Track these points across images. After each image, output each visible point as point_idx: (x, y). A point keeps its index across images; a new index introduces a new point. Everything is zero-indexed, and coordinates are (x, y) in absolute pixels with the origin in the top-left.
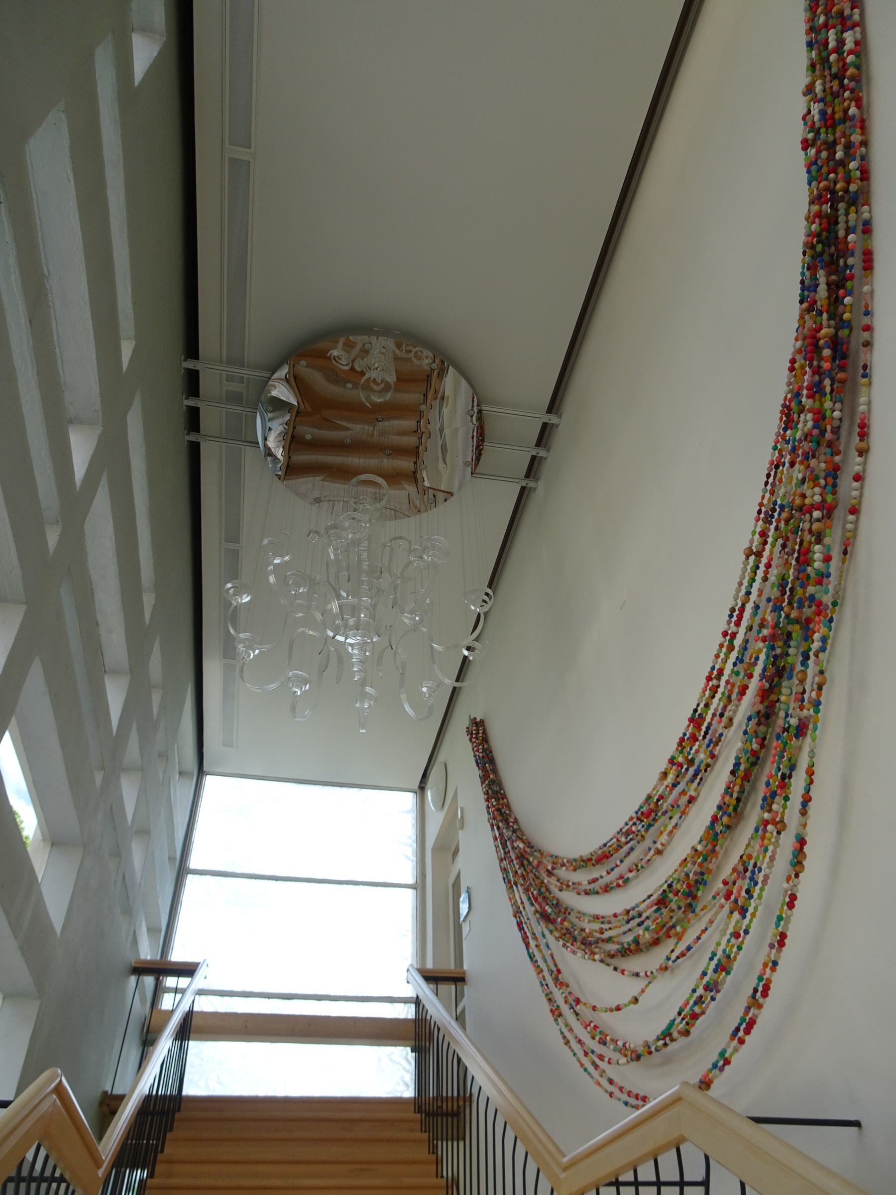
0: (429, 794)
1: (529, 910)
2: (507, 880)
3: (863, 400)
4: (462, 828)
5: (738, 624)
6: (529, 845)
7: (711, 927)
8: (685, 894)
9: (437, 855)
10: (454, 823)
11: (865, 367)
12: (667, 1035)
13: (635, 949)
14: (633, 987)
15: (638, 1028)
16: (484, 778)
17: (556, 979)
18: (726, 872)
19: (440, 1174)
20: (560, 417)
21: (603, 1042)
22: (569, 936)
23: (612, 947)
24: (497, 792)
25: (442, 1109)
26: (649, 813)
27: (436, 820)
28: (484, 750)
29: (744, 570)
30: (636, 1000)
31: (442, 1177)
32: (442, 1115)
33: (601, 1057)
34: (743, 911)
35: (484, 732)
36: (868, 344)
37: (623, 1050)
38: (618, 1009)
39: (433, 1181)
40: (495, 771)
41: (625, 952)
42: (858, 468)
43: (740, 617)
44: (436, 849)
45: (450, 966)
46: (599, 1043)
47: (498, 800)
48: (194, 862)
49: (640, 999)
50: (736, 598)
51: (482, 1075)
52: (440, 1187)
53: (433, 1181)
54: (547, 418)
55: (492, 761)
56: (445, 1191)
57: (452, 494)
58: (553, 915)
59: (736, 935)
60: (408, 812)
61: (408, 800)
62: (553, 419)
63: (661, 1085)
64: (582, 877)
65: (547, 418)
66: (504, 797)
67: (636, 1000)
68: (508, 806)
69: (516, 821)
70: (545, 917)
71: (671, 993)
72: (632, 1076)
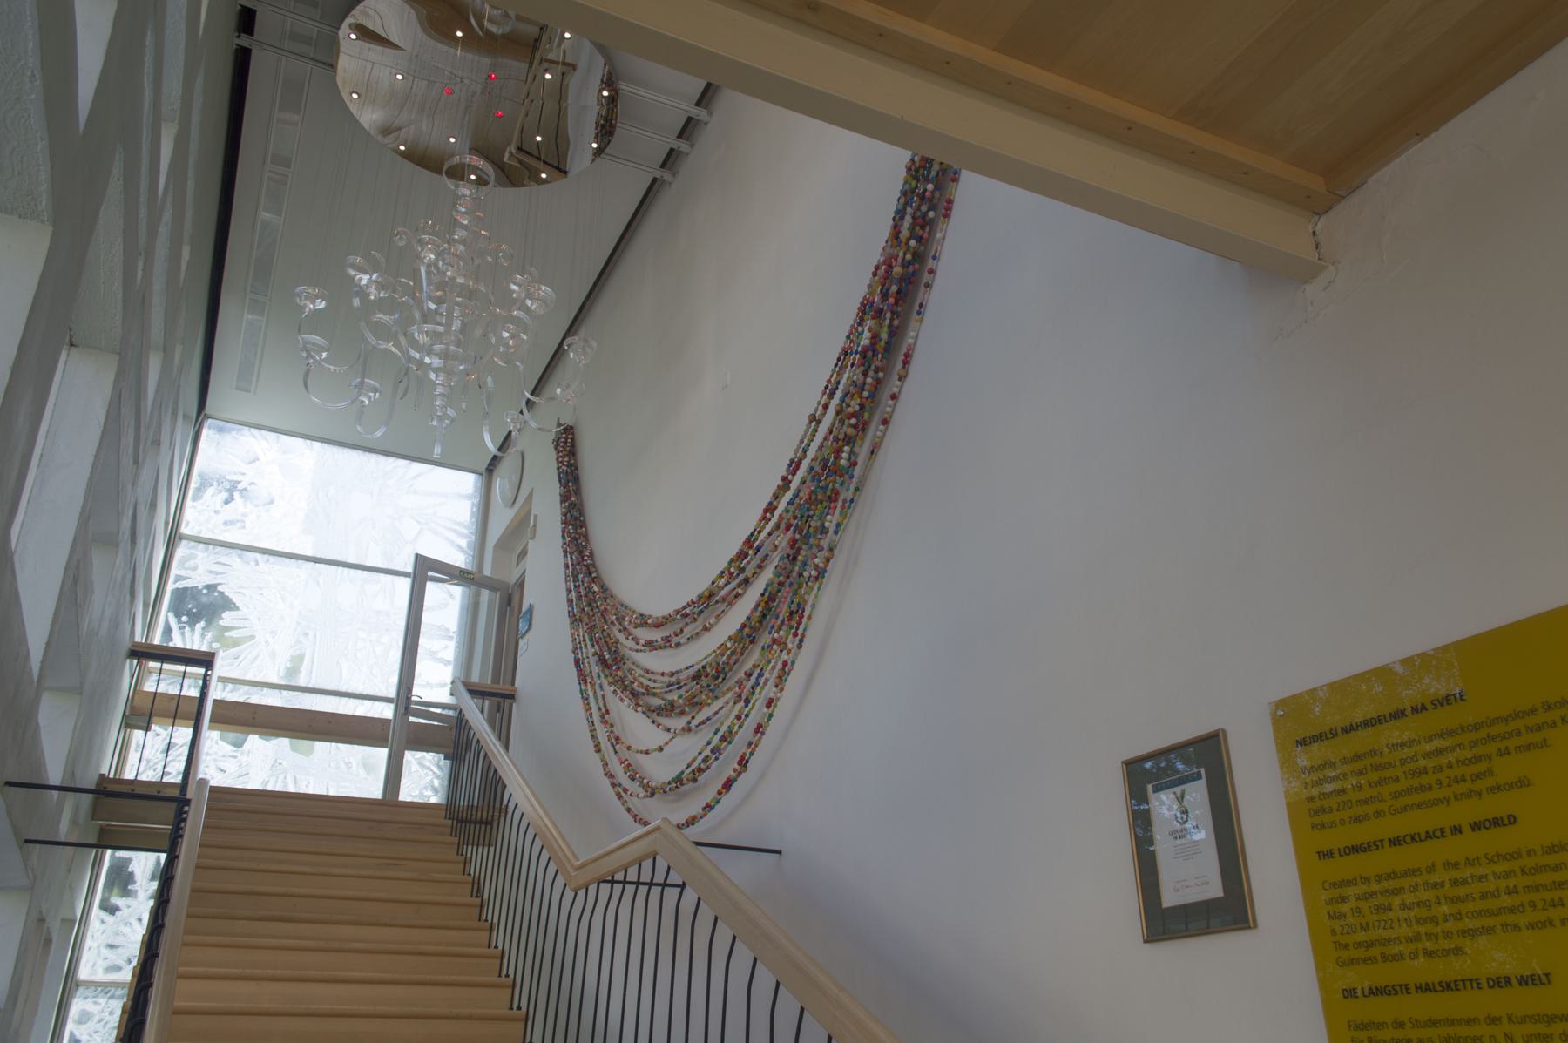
0: (498, 484)
1: (589, 651)
2: (572, 615)
3: (913, 334)
4: (533, 538)
5: (794, 473)
6: (604, 589)
7: (722, 709)
8: (710, 677)
9: (502, 539)
10: (521, 528)
11: (921, 305)
12: (678, 780)
13: (669, 709)
14: (660, 737)
15: (660, 770)
16: (565, 498)
17: (602, 717)
18: (748, 667)
19: (515, 1005)
20: (692, 146)
21: (632, 778)
22: (623, 685)
23: (657, 702)
24: (576, 519)
25: (476, 813)
26: (708, 598)
27: (502, 519)
28: (569, 465)
29: (806, 432)
30: (661, 749)
31: (519, 1008)
32: (481, 822)
33: (625, 790)
34: (747, 701)
35: (573, 445)
36: (928, 285)
37: (645, 787)
38: (647, 752)
39: (469, 900)
40: (578, 492)
41: (659, 711)
42: (895, 390)
43: (797, 467)
44: (502, 545)
45: (502, 687)
46: (630, 780)
47: (575, 528)
48: (184, 530)
49: (664, 749)
50: (796, 451)
51: (520, 792)
52: (516, 1020)
53: (494, 979)
54: (676, 143)
55: (576, 480)
56: (522, 1025)
57: (574, 67)
58: (612, 661)
59: (738, 717)
60: (468, 497)
61: (467, 482)
62: (683, 146)
63: (665, 813)
64: (645, 634)
65: (676, 143)
66: (583, 525)
67: (661, 749)
68: (586, 537)
69: (591, 555)
70: (602, 661)
71: (688, 748)
72: (640, 803)
